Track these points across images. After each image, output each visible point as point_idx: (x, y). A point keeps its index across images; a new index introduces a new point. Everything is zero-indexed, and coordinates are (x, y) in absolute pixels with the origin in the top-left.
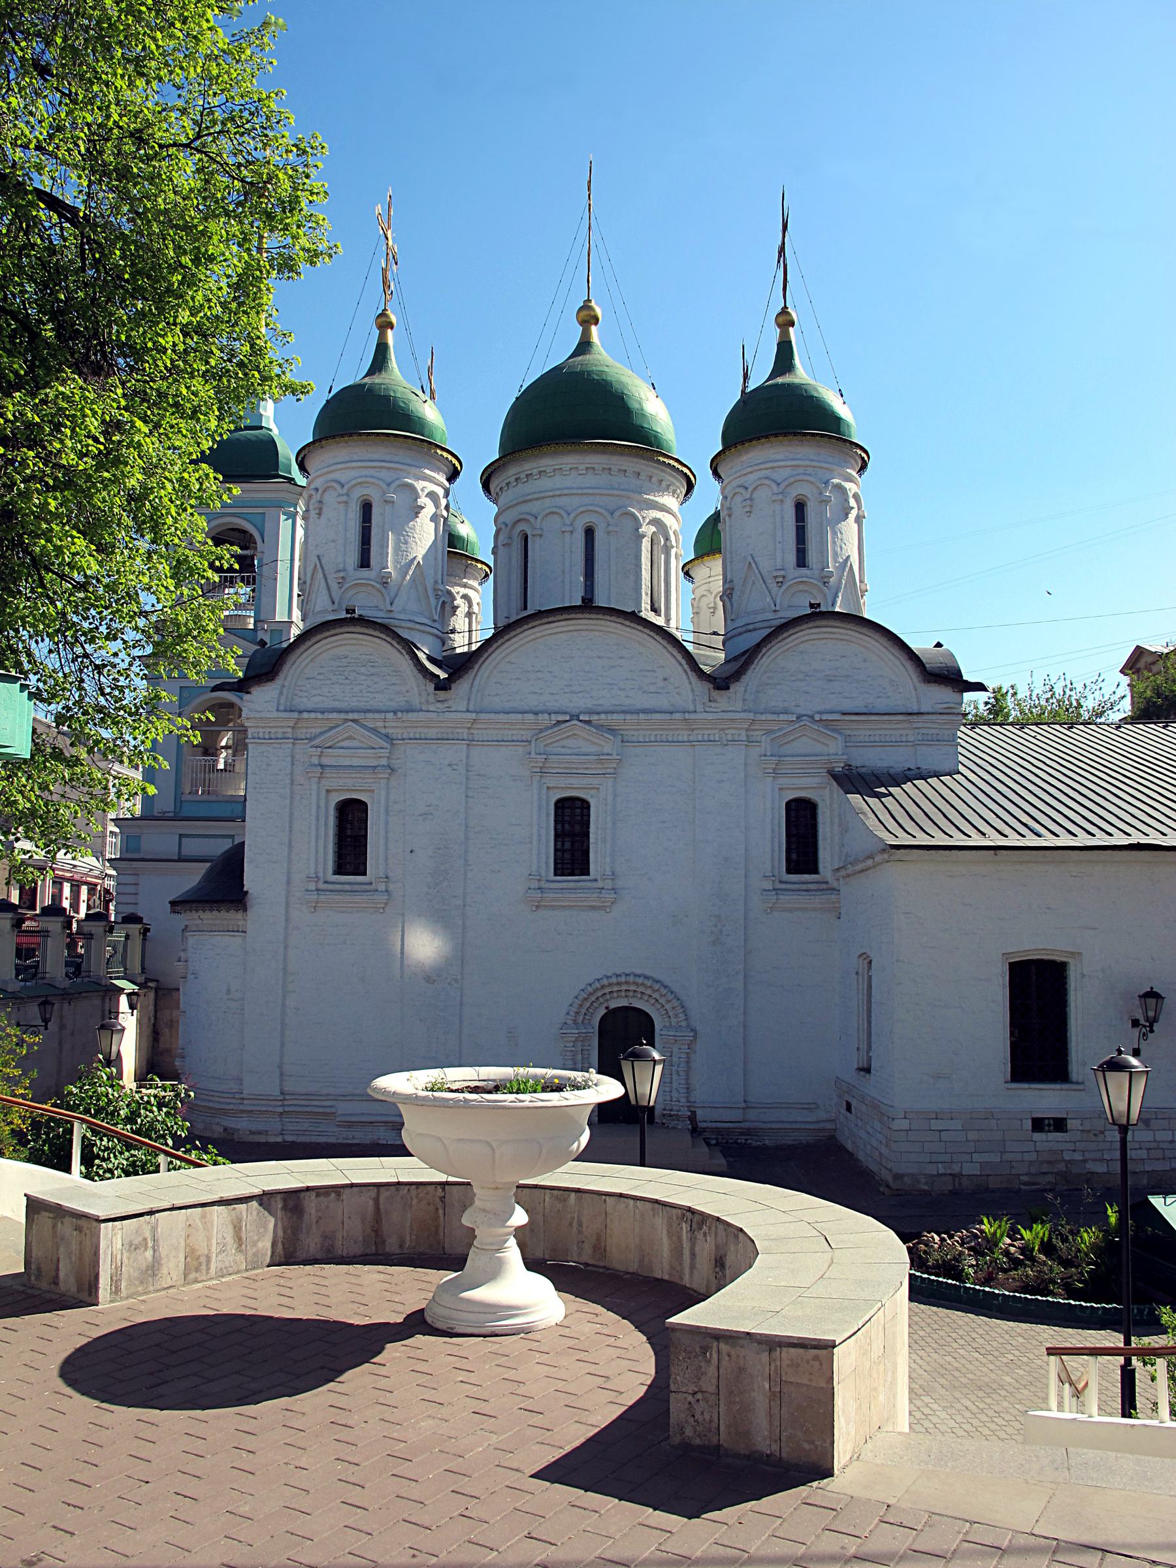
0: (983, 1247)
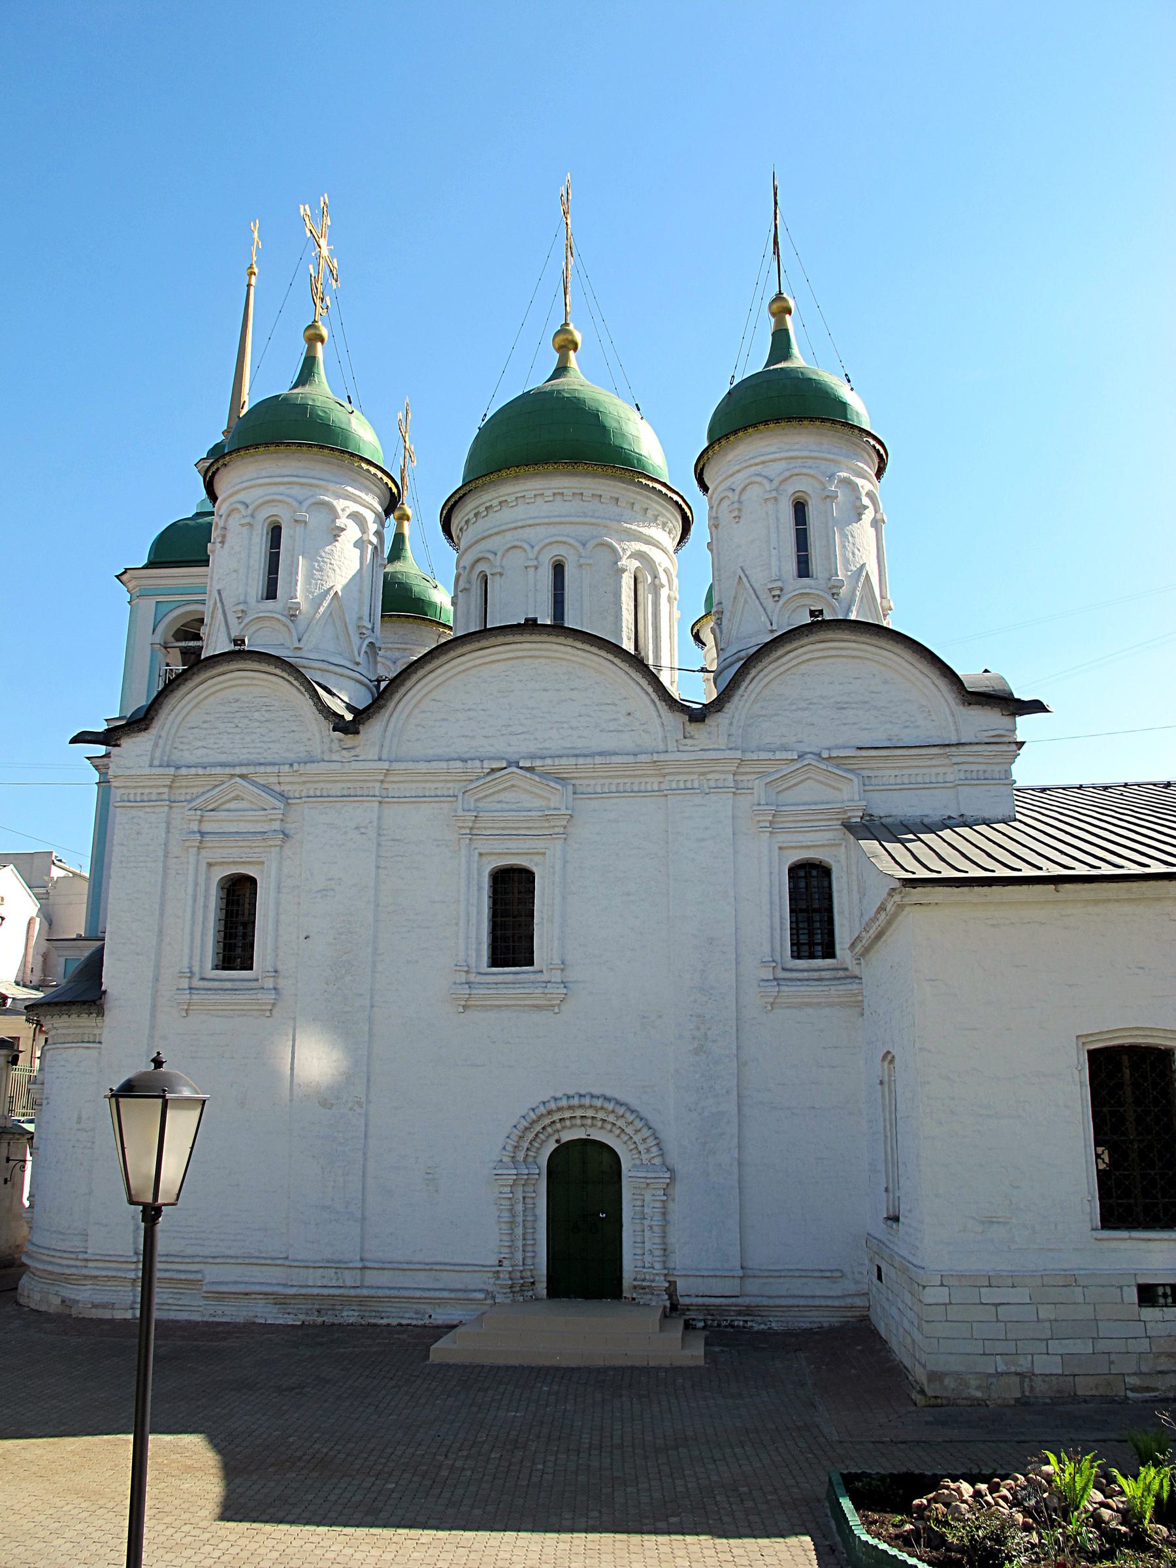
0: (1054, 1509)
